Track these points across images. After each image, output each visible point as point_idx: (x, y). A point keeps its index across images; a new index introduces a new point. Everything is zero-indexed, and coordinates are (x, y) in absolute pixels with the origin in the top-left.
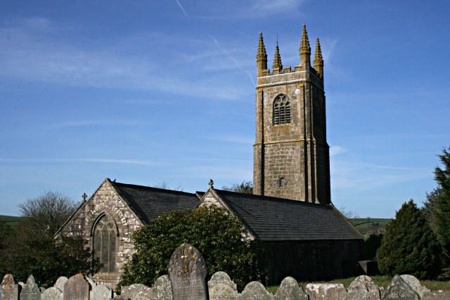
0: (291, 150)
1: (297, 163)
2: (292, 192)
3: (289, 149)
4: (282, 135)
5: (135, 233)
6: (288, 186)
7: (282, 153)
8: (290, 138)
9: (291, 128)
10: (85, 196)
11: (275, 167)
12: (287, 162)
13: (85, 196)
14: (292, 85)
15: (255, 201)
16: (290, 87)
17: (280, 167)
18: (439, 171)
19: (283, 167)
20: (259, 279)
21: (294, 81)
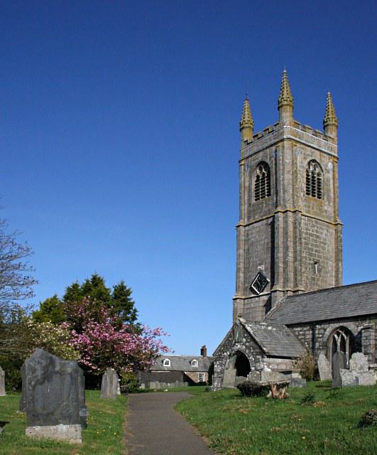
0: (325, 232)
1: (330, 248)
2: (326, 282)
3: (323, 229)
4: (315, 210)
5: (44, 367)
6: (322, 274)
7: (317, 232)
8: (323, 216)
9: (325, 205)
10: (203, 351)
11: (310, 247)
12: (322, 245)
13: (203, 351)
14: (326, 155)
15: (334, 295)
16: (324, 157)
17: (315, 249)
18: (75, 286)
19: (318, 249)
20: (38, 318)
21: (326, 151)
